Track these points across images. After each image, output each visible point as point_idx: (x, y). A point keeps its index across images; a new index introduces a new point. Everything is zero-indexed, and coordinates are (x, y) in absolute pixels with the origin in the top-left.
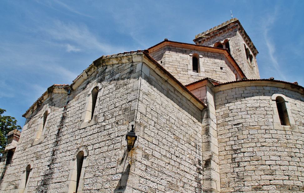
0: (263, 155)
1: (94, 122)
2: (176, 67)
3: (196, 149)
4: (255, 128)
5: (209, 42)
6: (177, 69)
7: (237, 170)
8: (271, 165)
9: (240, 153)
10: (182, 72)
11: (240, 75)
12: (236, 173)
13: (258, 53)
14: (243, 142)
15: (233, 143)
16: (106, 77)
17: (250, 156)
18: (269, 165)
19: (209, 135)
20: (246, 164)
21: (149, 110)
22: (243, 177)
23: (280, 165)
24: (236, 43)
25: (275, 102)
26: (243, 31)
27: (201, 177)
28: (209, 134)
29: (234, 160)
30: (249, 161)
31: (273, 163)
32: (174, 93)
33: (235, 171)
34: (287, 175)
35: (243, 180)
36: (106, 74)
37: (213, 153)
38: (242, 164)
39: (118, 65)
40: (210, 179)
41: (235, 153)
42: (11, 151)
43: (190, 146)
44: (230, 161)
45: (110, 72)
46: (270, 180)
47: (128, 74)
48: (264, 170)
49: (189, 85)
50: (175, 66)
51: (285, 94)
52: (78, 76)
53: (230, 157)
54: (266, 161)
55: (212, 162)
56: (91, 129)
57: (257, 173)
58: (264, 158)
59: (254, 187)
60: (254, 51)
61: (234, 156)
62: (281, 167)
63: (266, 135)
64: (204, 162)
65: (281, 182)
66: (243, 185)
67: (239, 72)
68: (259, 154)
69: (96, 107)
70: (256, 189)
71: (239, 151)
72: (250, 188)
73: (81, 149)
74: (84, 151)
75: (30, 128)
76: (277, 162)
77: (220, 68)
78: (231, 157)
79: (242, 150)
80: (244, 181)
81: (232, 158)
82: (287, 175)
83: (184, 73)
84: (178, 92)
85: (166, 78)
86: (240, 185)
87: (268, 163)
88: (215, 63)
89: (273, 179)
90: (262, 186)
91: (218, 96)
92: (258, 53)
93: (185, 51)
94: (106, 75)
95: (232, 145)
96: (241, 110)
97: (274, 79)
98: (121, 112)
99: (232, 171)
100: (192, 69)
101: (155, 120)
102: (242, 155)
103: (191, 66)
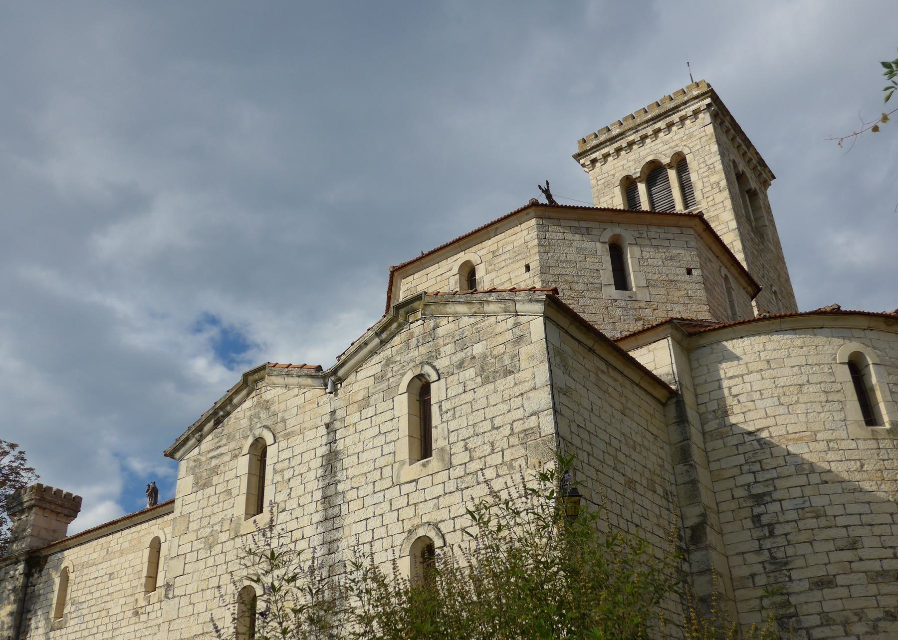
0: (828, 502)
1: (440, 464)
2: (569, 278)
3: (668, 501)
4: (801, 439)
5: (625, 161)
6: (573, 285)
7: (768, 544)
8: (850, 526)
9: (771, 502)
10: (587, 294)
11: (737, 274)
12: (766, 553)
13: (774, 178)
14: (775, 476)
15: (750, 478)
16: (441, 349)
17: (797, 509)
18: (846, 527)
19: (691, 465)
20: (788, 528)
21: (574, 428)
22: (785, 560)
23: (871, 525)
24: (709, 162)
25: (847, 366)
26: (728, 118)
27: (686, 567)
28: (692, 462)
29: (759, 521)
30: (796, 521)
31: (855, 520)
32: (609, 375)
33: (764, 547)
34: (891, 547)
35: (788, 567)
36: (441, 341)
37: (706, 508)
38: (779, 530)
39: (472, 320)
40: (707, 571)
41: (759, 505)
42: (38, 554)
43: (656, 495)
44: (749, 523)
45: (453, 337)
46: (850, 562)
47: (509, 345)
48: (834, 539)
49: (626, 337)
50: (567, 278)
51: (870, 344)
52: (353, 344)
53: (746, 513)
54: (835, 516)
55: (708, 529)
56: (436, 481)
57: (818, 547)
58: (830, 511)
59: (815, 580)
60: (760, 174)
61: (758, 510)
62: (875, 529)
63: (830, 453)
64: (689, 532)
65: (876, 566)
66: (787, 579)
67: (733, 269)
68: (817, 502)
69: (436, 427)
70: (819, 585)
71: (767, 498)
72: (806, 585)
73: (421, 532)
74: (432, 534)
75: (205, 486)
76: (866, 519)
77: (685, 271)
78: (749, 514)
79: (776, 496)
80: (789, 570)
81: (753, 517)
82: (891, 547)
83: (594, 294)
84: (615, 368)
85: (590, 343)
86: (781, 580)
87: (841, 521)
88: (672, 259)
89: (857, 559)
90: (834, 576)
91: (698, 360)
92: (774, 178)
93: (588, 229)
94: (442, 343)
95: (749, 485)
96: (761, 394)
97: (839, 307)
98: (514, 440)
99: (756, 545)
100: (612, 281)
101: (587, 447)
102: (775, 507)
103: (607, 275)
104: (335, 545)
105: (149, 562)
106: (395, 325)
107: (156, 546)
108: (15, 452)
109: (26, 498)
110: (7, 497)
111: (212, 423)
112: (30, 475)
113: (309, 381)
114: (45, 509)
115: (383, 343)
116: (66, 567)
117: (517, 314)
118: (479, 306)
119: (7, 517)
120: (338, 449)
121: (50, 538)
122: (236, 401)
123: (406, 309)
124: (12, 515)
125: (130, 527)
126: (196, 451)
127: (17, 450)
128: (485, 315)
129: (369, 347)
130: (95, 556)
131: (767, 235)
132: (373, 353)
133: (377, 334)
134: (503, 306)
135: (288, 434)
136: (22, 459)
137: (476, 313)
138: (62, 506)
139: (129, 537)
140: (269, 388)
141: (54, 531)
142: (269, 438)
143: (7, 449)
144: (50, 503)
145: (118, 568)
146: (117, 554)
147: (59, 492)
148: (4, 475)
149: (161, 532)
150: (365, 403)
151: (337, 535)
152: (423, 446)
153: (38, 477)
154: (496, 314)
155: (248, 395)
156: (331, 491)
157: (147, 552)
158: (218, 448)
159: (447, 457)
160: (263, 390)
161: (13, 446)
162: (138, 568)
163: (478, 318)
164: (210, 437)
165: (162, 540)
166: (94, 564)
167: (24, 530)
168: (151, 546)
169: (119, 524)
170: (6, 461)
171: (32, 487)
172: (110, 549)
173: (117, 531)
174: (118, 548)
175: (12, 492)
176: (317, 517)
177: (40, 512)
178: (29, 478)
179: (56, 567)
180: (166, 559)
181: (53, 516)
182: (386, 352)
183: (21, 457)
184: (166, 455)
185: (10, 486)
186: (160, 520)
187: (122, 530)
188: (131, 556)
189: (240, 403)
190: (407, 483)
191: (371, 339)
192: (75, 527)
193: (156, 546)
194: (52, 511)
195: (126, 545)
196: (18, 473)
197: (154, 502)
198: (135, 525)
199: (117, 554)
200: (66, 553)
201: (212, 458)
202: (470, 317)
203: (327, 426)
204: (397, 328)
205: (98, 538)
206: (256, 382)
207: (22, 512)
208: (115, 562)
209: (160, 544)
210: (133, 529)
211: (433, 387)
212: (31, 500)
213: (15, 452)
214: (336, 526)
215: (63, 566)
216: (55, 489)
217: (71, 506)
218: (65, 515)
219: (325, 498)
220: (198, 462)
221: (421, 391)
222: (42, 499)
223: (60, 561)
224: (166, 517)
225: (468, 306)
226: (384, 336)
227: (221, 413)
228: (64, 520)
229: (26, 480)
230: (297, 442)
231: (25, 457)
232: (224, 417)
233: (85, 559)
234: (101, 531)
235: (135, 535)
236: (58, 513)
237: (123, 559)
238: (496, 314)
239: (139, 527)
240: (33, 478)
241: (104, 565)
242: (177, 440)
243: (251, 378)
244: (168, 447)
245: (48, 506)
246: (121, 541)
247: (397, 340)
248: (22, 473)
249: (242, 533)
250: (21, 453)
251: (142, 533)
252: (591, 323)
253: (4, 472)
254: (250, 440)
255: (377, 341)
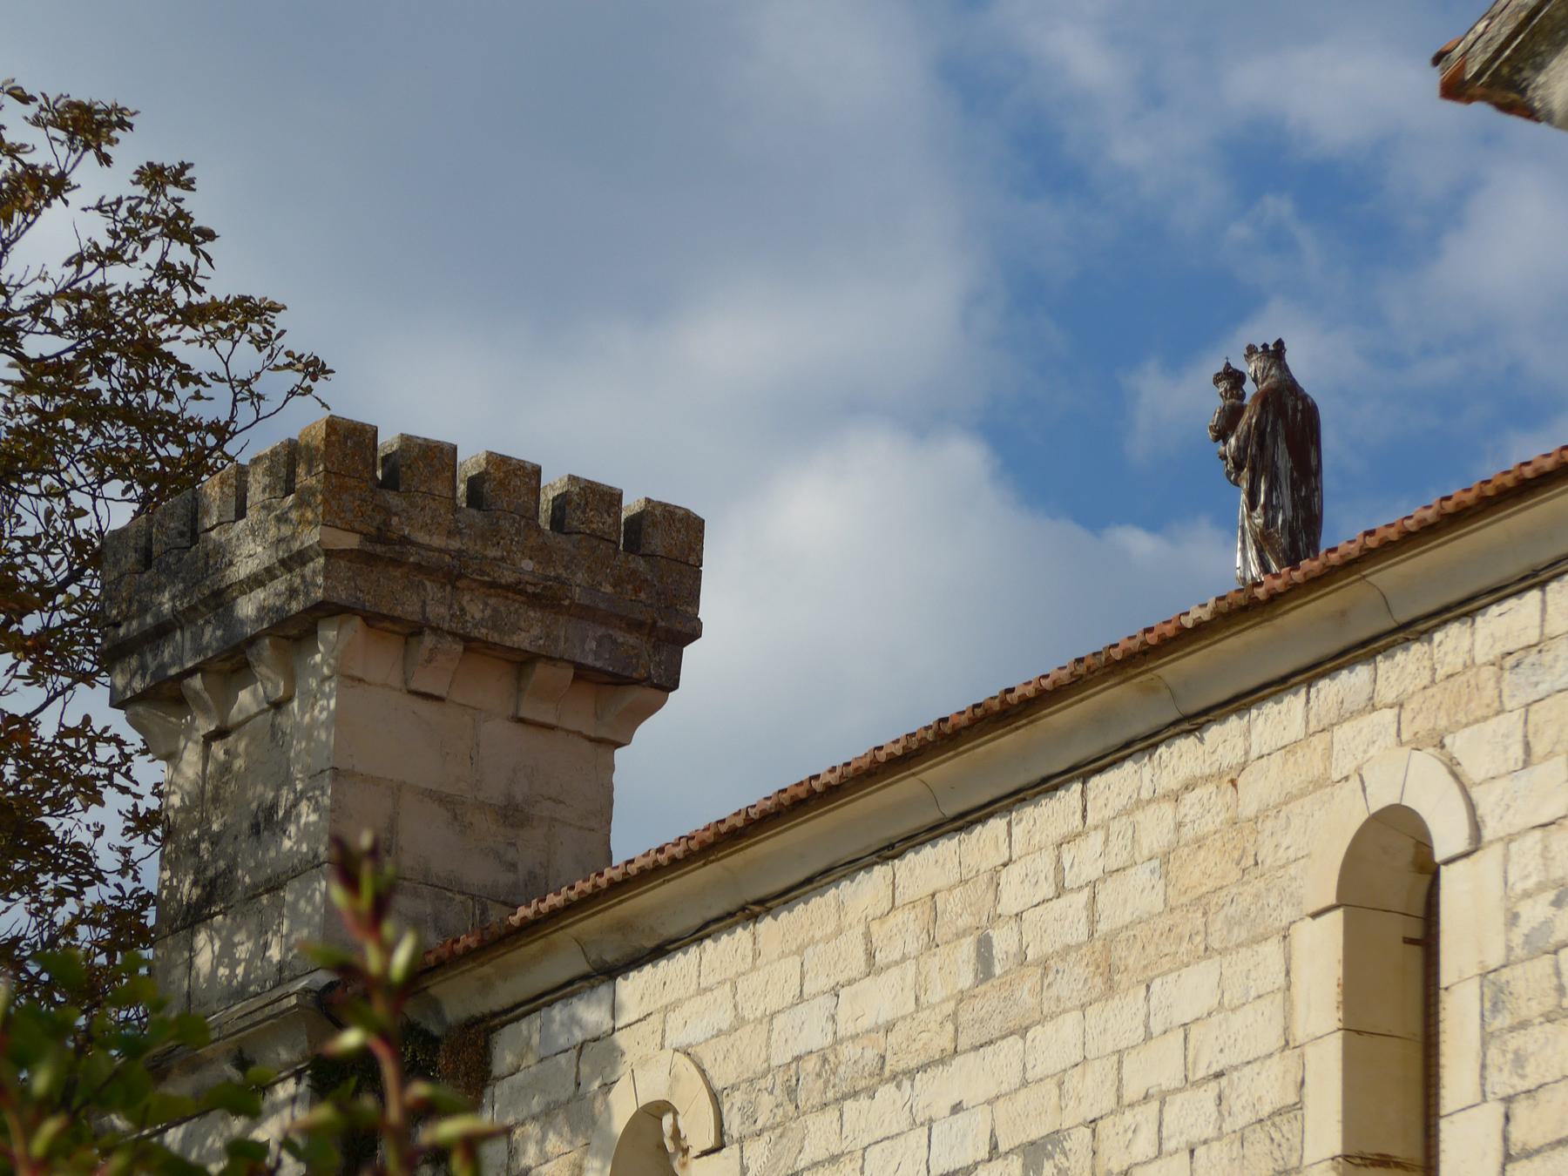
105: (1353, 1031)
107: (1395, 893)
108: (99, 181)
109: (250, 553)
110: (92, 553)
112: (245, 358)
114: (412, 631)
116: (655, 1111)
119: (118, 722)
121: (480, 873)
124: (156, 702)
125: (1145, 744)
127: (130, 152)
130: (879, 1000)
131: (482, 965)
136: (179, 228)
138: (546, 599)
139: (1155, 828)
141: (512, 815)
143: (46, 151)
144: (452, 575)
145: (1092, 1093)
146: (1070, 982)
147: (509, 479)
148: (36, 373)
149: (1426, 765)
153: (316, 369)
157: (1321, 947)
161: (88, 126)
162: (1265, 1087)
165: (1447, 837)
166: (883, 1074)
167: (267, 822)
168: (1354, 896)
169: (1060, 718)
170: (47, 247)
171: (292, 455)
172: (1003, 941)
173: (1047, 785)
174: (1066, 921)
175: (116, 510)
177: (381, 663)
178: (244, 389)
179: (575, 1109)
180: (1495, 996)
181: (488, 690)
183: (161, 209)
184: (1454, 89)
185: (106, 464)
186: (1402, 669)
187: (1084, 770)
188: (1188, 991)
192: (671, 774)
193: (1395, 893)
194: (472, 645)
195: (1135, 897)
196: (147, 350)
197: (1294, 532)
198: (1194, 722)
199: (1070, 982)
200: (634, 988)
205: (889, 851)
207: (234, 663)
208: (1055, 1043)
209: (1428, 872)
210: (1181, 758)
212: (294, 561)
213: (99, 181)
215: (622, 1108)
216: (470, 458)
217: (609, 591)
218: (582, 674)
222: (381, 551)
223: (599, 1051)
224: (1452, 641)
228: (579, 715)
229: (214, 407)
231: (199, 207)
233: (807, 1032)
234: (903, 788)
235: (1205, 810)
236: (522, 663)
237: (1121, 1019)
239: (1226, 738)
240: (275, 385)
241: (970, 1078)
245: (433, 603)
246: (1085, 861)
248: (185, 346)
250: (154, 176)
251: (1257, 790)
253: (38, 345)
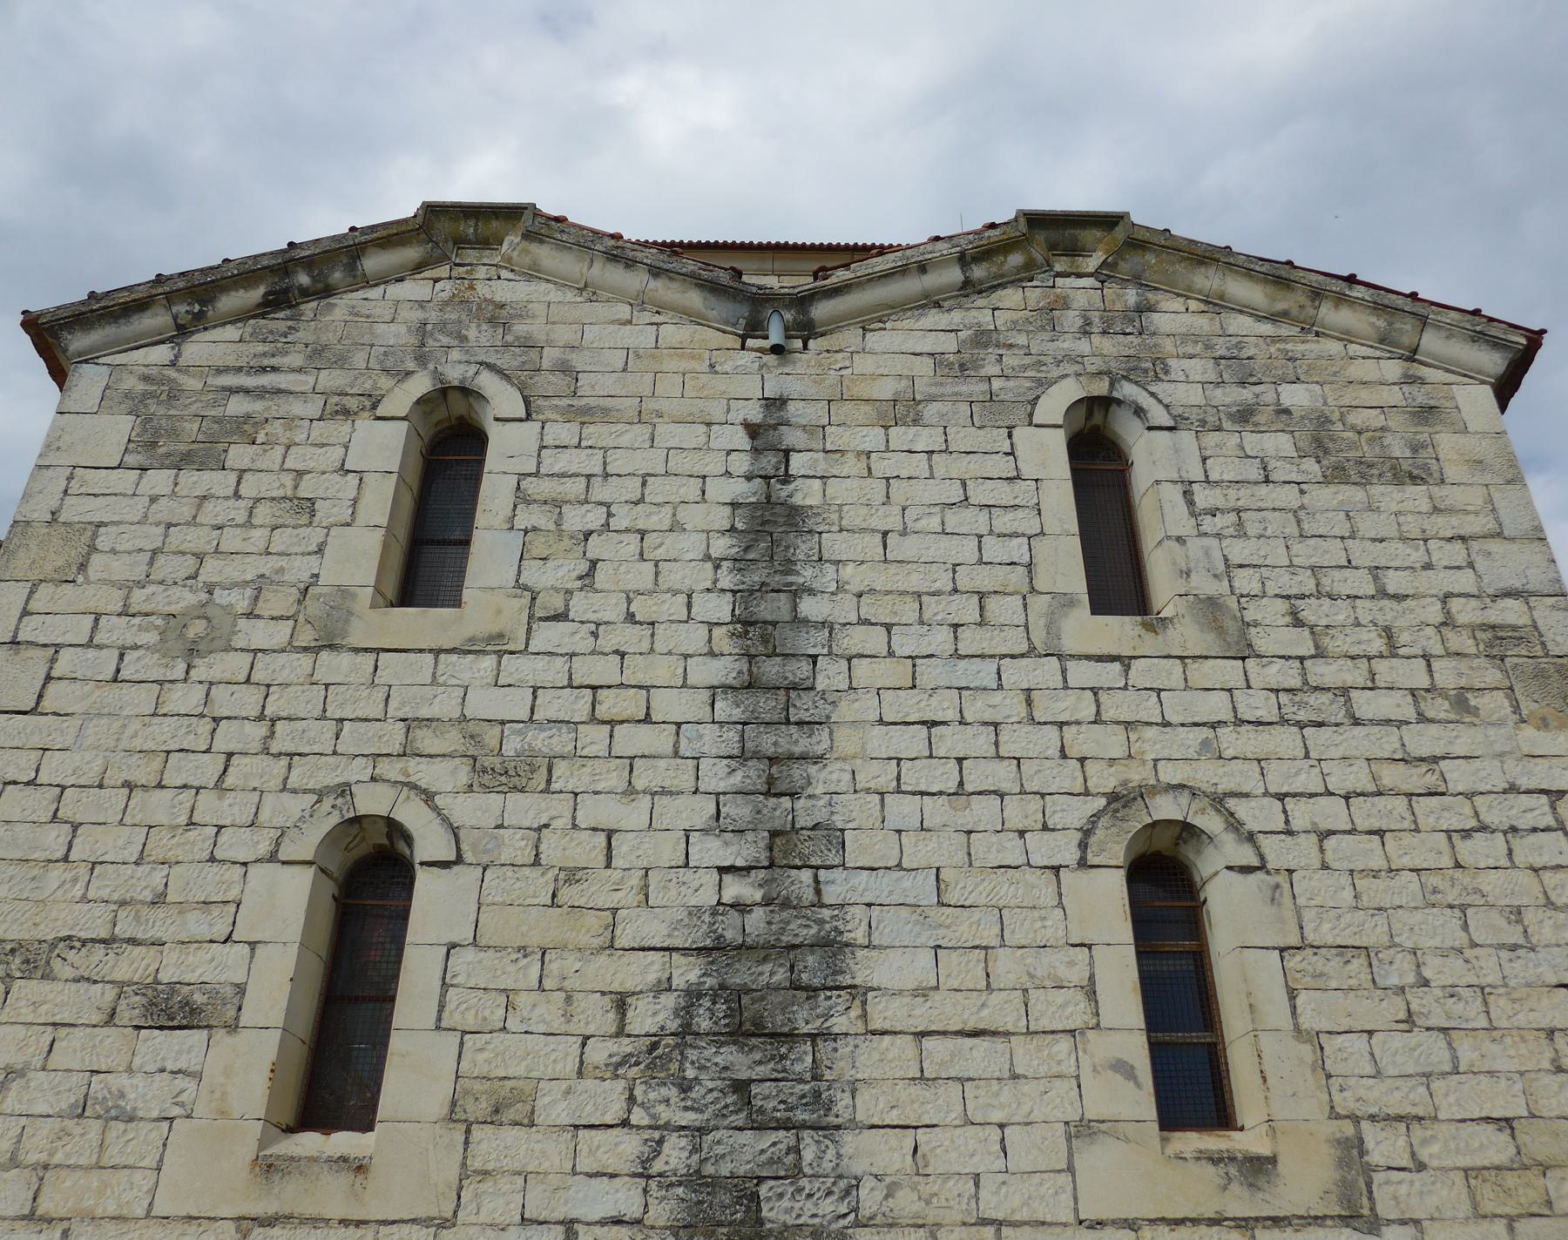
39: (1267, 328)
104: (797, 771)
106: (1016, 259)
111: (256, 294)
113: (694, 299)
115: (969, 288)
117: (1412, 356)
118: (1303, 300)
120: (798, 500)
122: (373, 263)
123: (1054, 235)
126: (162, 353)
128: (1312, 329)
129: (932, 280)
132: (931, 301)
133: (964, 260)
134: (1381, 323)
135: (587, 410)
137: (1285, 314)
140: (505, 274)
142: (501, 398)
150: (903, 410)
151: (803, 743)
152: (1118, 581)
154: (1347, 337)
155: (418, 268)
156: (773, 608)
158: (263, 370)
159: (1231, 626)
160: (481, 272)
163: (1285, 330)
164: (231, 332)
176: (724, 670)
182: (978, 313)
189: (383, 280)
190: (1089, 658)
191: (942, 262)
201: (233, 391)
202: (1259, 318)
203: (753, 430)
204: (1019, 269)
206: (460, 242)
211: (426, 884)
214: (113, 1156)
219: (747, 623)
220: (163, 388)
221: (1096, 454)
225: (1270, 289)
226: (978, 272)
227: (304, 279)
230: (625, 440)
232: (306, 294)
238: (1347, 337)
242: (92, 295)
243: (444, 227)
244: (44, 300)
247: (1010, 297)
249: (355, 639)
252: (1178, 1134)
254: (421, 385)
255: (954, 275)
